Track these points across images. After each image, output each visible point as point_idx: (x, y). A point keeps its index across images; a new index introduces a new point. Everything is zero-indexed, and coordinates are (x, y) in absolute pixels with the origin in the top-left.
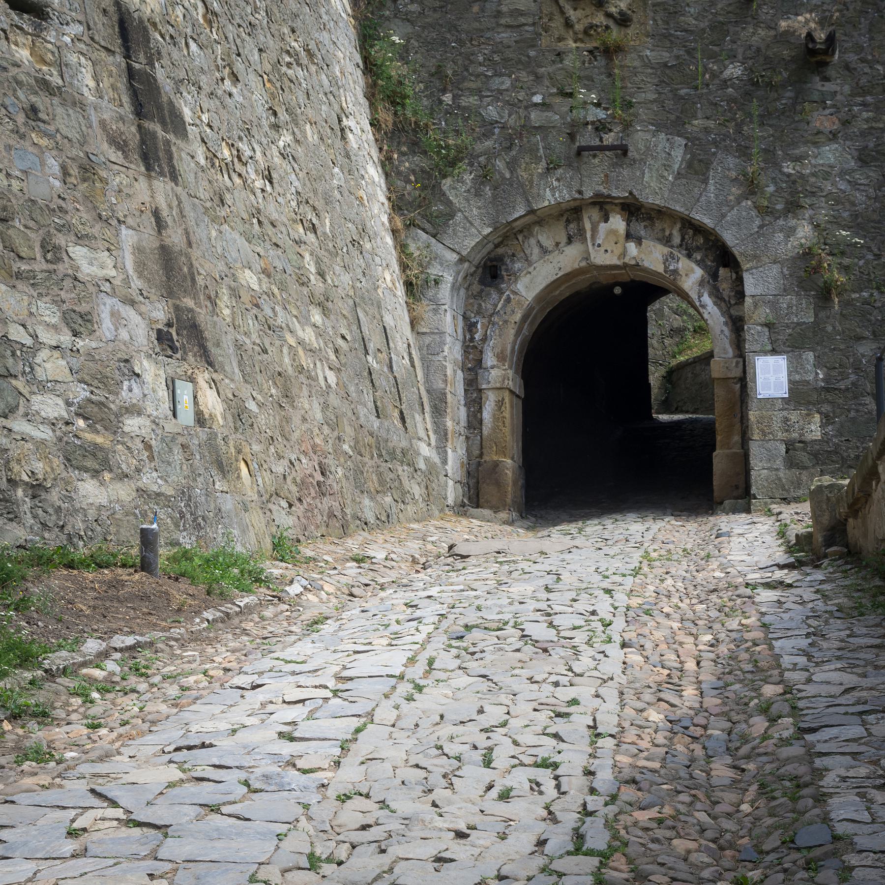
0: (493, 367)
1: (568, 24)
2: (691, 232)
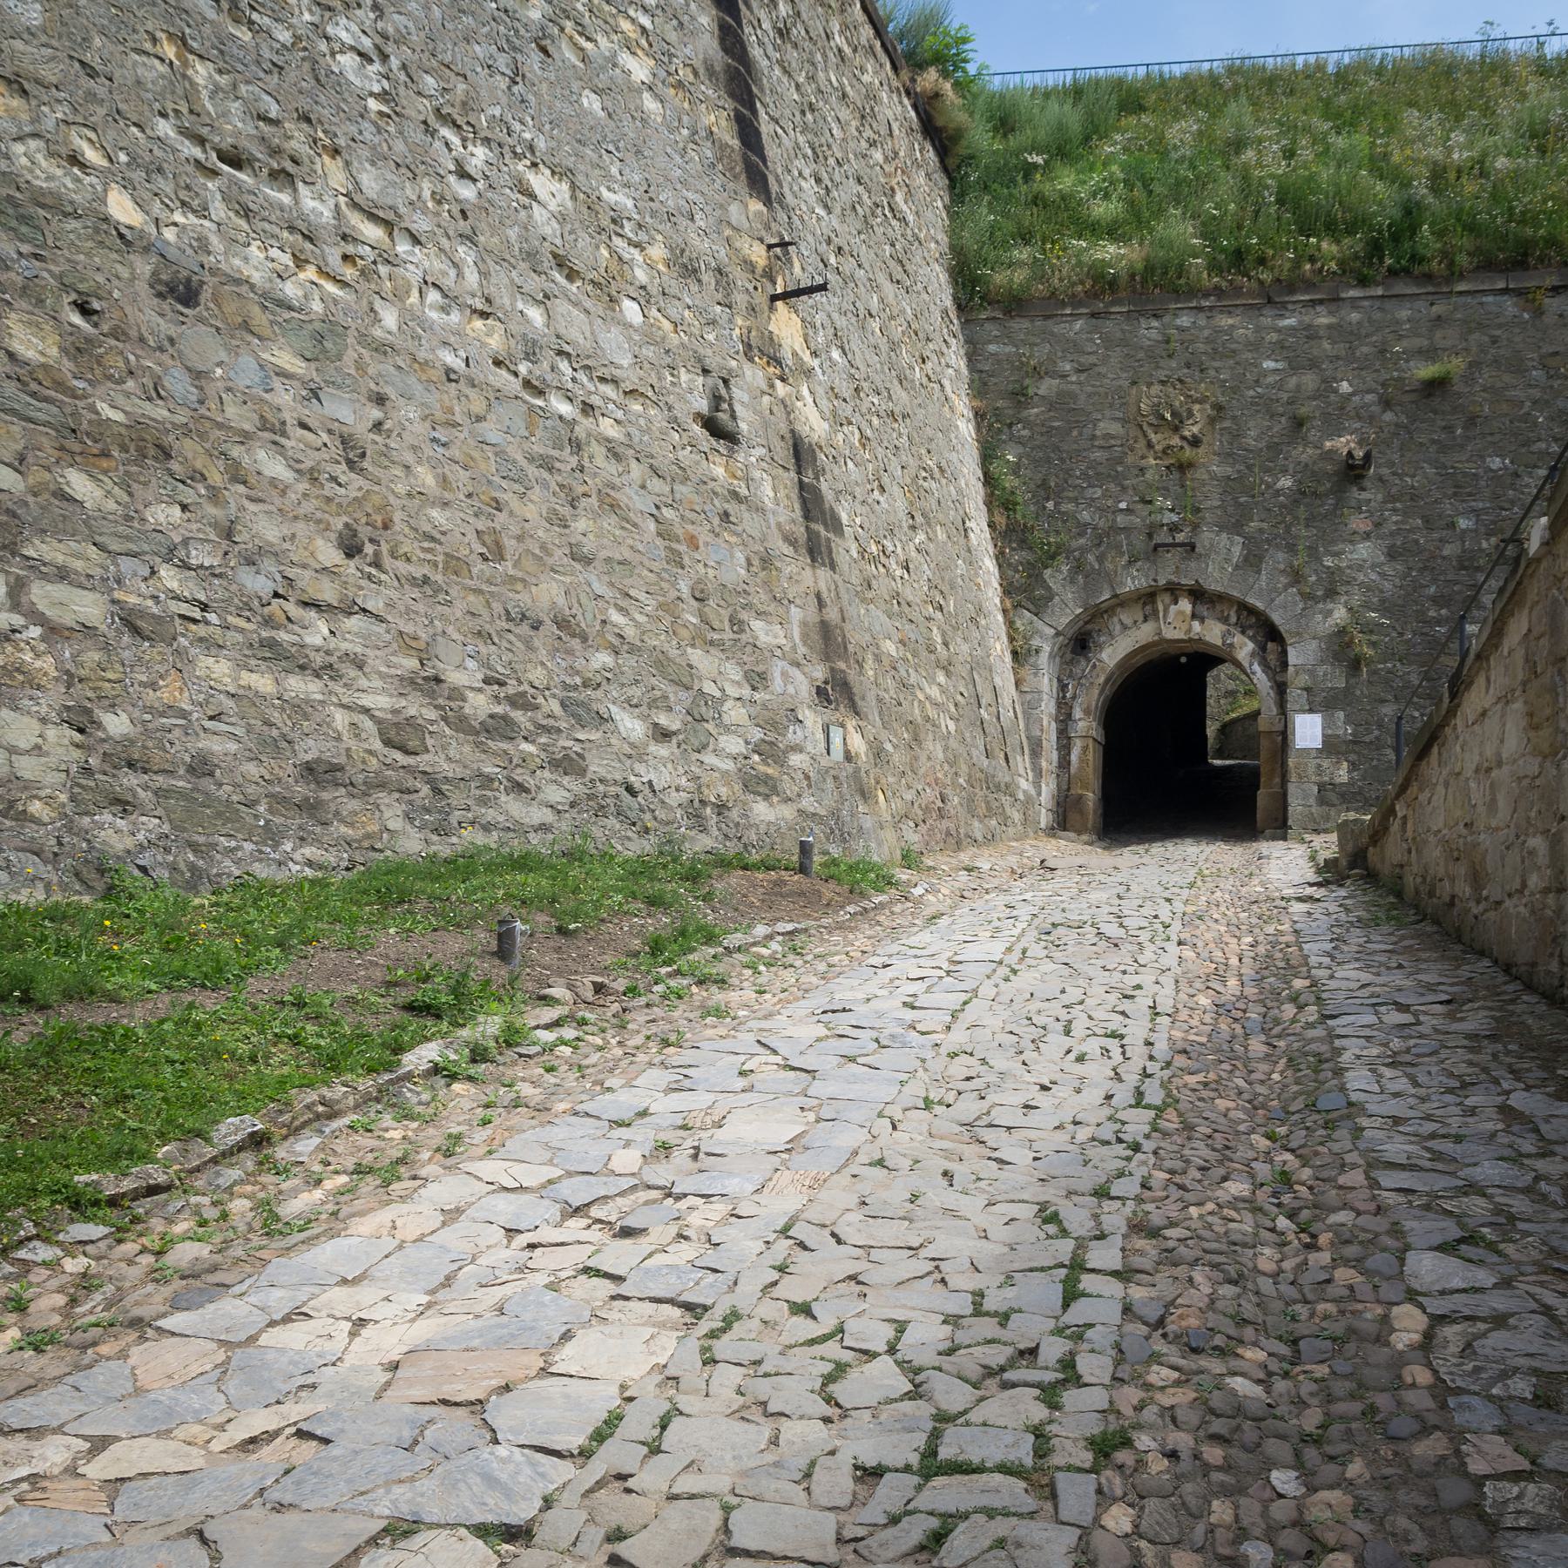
1: (1150, 445)
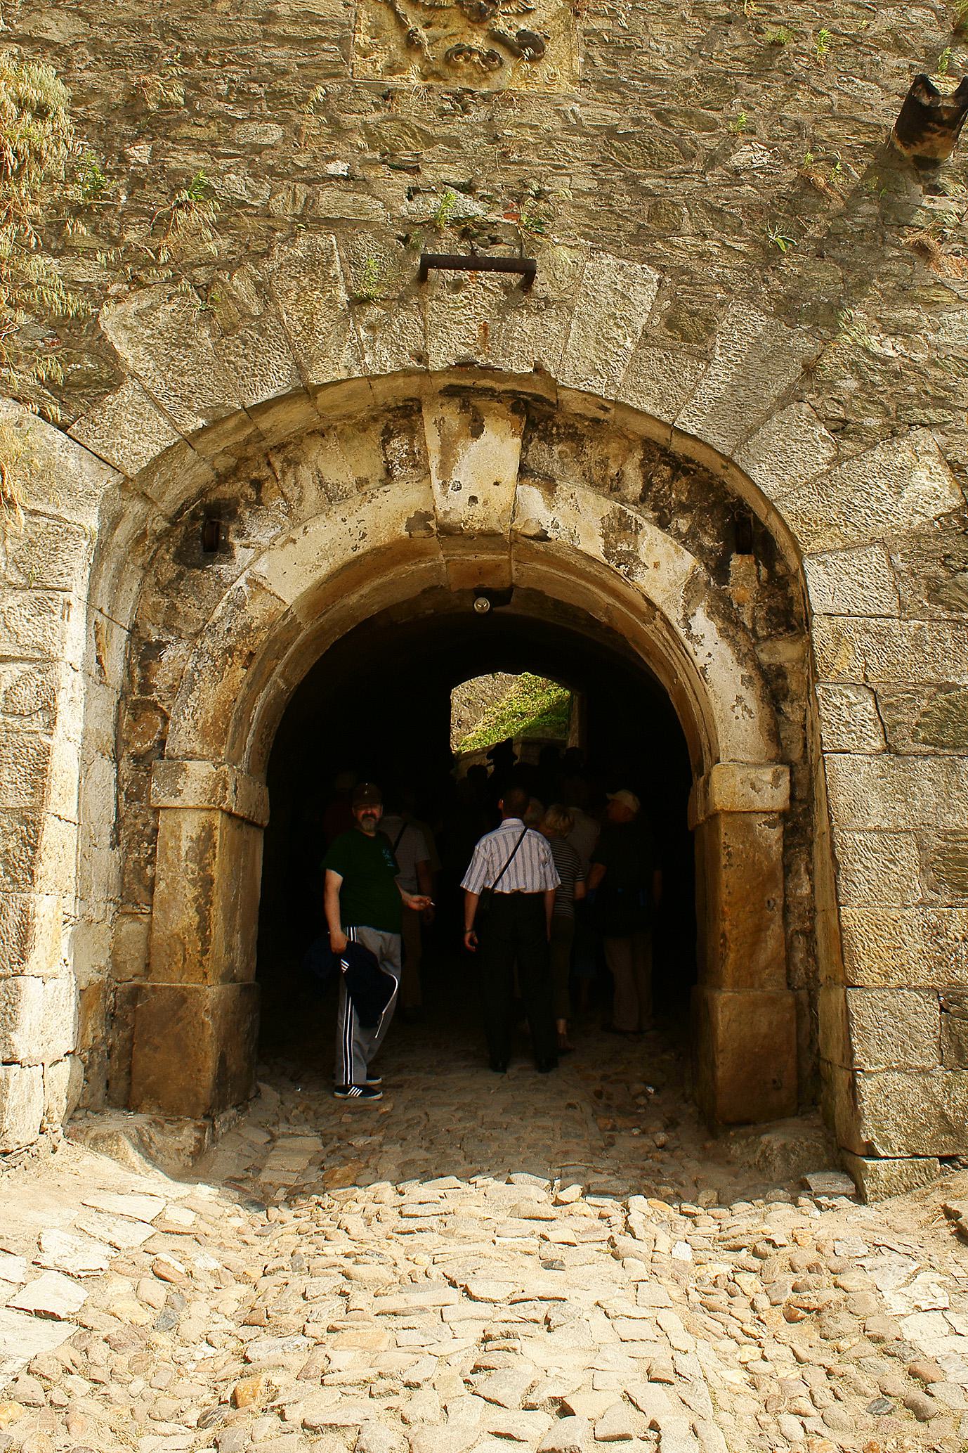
0: (191, 756)
1: (411, 43)
2: (666, 472)
